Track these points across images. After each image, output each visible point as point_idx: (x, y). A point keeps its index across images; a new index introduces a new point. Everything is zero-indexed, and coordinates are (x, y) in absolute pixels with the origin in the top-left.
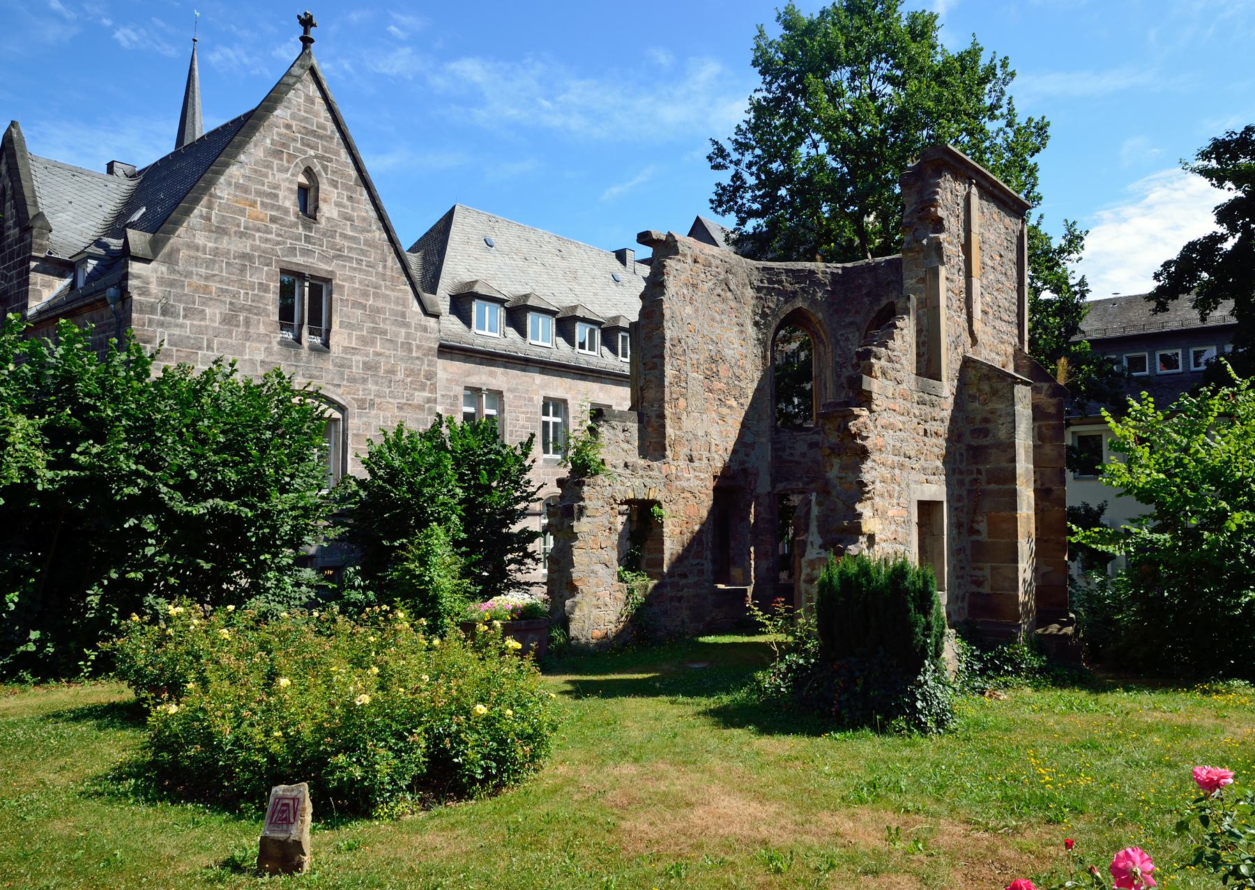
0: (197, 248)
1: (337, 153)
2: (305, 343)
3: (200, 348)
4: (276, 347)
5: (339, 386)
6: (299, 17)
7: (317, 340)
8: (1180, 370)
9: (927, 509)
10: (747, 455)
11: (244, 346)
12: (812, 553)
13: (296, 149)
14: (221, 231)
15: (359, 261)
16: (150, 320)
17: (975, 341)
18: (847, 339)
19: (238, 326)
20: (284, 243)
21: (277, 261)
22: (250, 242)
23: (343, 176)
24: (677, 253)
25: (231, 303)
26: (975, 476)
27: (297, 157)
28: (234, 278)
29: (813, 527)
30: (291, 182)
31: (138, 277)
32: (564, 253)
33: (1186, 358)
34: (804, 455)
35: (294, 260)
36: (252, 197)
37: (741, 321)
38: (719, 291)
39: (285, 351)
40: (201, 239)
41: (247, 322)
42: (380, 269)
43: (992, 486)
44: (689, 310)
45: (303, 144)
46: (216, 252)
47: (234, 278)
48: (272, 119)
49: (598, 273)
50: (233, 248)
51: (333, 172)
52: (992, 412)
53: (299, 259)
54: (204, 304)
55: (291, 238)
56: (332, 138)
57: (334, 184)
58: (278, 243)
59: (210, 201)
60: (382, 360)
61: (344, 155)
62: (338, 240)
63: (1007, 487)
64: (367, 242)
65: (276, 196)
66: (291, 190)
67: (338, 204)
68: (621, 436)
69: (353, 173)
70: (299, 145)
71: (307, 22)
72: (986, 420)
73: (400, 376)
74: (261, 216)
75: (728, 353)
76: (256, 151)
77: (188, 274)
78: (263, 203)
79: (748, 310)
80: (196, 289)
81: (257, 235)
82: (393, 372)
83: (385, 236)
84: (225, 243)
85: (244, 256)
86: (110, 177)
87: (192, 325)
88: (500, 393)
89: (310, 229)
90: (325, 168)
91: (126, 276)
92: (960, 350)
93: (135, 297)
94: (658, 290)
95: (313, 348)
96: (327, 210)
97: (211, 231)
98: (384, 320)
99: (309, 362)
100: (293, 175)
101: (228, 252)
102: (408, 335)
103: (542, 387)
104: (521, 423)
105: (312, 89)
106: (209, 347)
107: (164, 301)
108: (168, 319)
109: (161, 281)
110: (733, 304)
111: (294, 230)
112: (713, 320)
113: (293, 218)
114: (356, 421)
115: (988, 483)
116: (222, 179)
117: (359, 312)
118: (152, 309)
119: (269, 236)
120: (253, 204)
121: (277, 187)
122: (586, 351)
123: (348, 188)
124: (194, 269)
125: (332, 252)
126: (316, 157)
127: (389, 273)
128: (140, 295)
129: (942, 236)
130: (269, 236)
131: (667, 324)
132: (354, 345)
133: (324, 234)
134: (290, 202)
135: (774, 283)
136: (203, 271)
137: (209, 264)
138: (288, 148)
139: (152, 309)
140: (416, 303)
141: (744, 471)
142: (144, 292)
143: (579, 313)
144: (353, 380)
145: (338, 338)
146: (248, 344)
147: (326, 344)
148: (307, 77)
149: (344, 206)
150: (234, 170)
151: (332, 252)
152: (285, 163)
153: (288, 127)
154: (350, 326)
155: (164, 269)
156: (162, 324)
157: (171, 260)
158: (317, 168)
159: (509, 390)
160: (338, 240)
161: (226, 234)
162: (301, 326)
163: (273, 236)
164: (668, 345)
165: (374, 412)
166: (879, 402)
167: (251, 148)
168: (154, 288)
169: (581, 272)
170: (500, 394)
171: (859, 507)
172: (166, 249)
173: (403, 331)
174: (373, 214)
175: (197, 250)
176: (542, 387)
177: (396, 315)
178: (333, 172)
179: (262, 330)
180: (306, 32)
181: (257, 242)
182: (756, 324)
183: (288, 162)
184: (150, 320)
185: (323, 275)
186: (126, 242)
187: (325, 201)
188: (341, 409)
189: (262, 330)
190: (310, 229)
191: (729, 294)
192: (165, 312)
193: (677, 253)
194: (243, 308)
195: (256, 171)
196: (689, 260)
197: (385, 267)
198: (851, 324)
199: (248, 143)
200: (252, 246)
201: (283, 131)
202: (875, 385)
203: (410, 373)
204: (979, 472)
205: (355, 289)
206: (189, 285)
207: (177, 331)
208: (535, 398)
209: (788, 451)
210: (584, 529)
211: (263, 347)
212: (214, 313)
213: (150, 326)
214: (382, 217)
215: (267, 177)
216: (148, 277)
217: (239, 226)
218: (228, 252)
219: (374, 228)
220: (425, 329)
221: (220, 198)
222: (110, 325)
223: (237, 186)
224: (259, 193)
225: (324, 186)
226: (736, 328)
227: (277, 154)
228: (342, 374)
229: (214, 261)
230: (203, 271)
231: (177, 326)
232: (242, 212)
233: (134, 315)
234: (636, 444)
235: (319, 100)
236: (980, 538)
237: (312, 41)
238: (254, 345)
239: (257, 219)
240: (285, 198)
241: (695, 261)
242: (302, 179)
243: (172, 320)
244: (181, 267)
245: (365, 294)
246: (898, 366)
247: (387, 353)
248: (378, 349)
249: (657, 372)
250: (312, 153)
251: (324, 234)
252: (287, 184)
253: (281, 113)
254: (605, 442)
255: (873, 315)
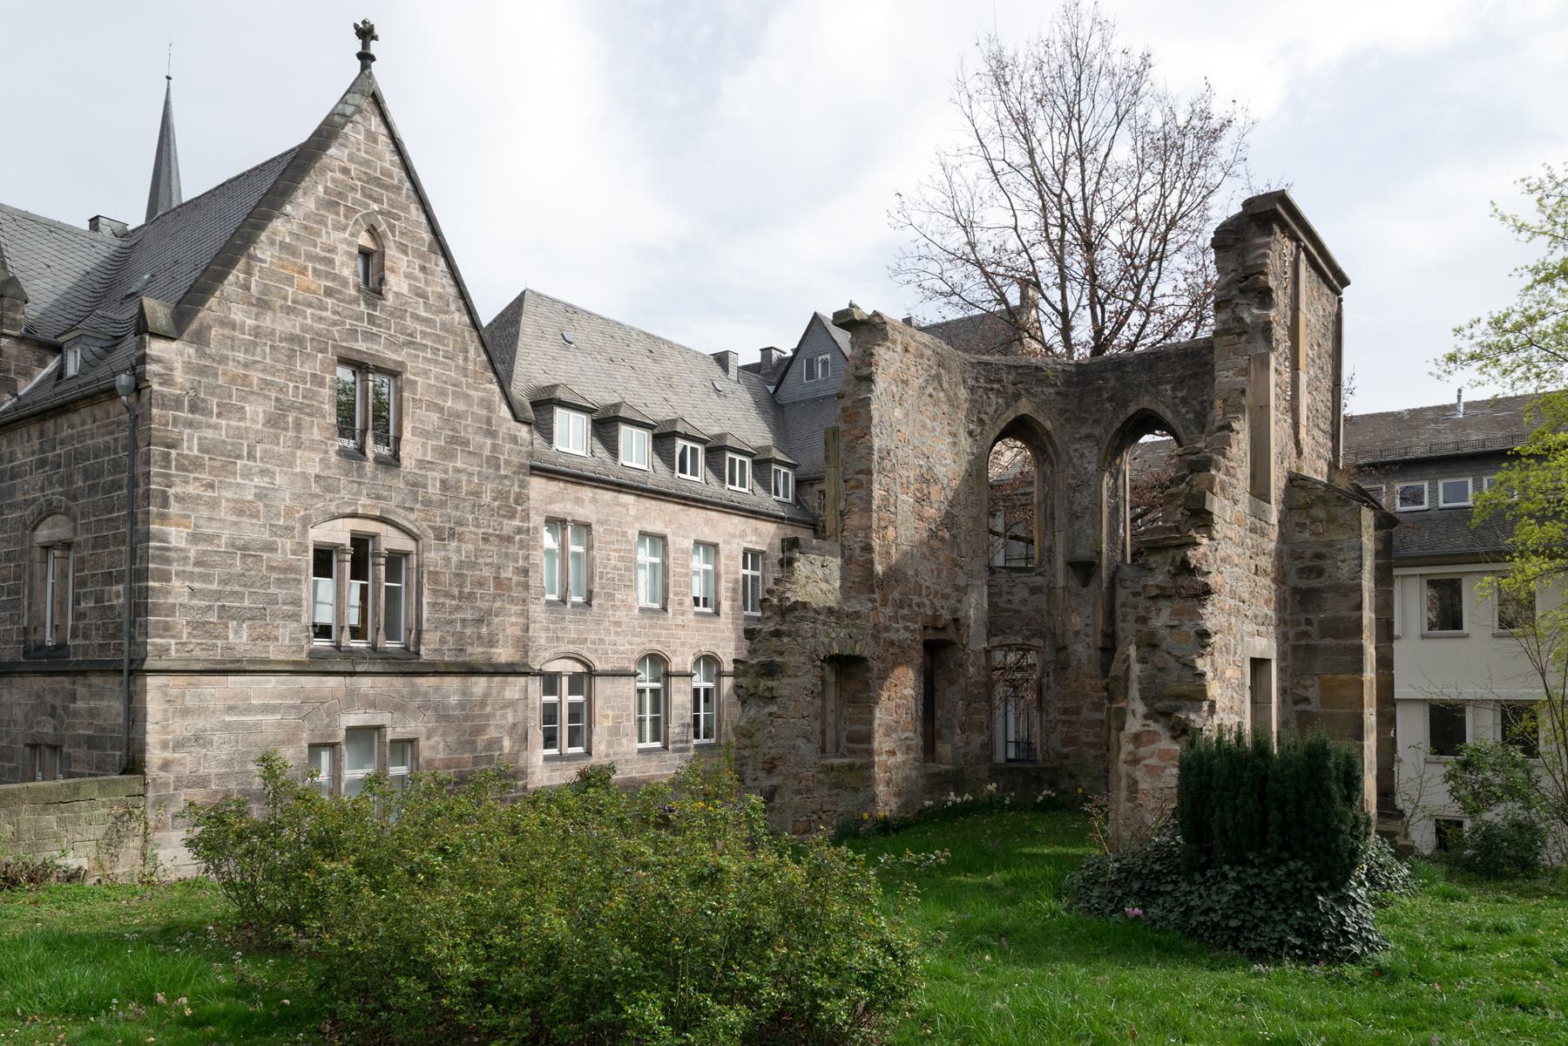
0: (233, 326)
1: (406, 209)
2: (370, 455)
3: (239, 457)
4: (334, 458)
5: (412, 509)
6: (356, 26)
7: (385, 451)
8: (1426, 506)
9: (1258, 665)
10: (959, 601)
11: (293, 455)
12: (1134, 725)
13: (355, 201)
14: (262, 305)
15: (435, 351)
16: (175, 419)
17: (1300, 453)
18: (1082, 456)
19: (286, 429)
20: (343, 323)
21: (334, 347)
22: (300, 319)
23: (415, 239)
24: (885, 338)
25: (277, 399)
26: (1303, 628)
27: (356, 211)
28: (280, 366)
29: (1134, 691)
30: (350, 244)
31: (158, 361)
32: (656, 355)
33: (1433, 491)
34: (1024, 602)
35: (356, 346)
36: (301, 261)
37: (953, 430)
38: (930, 390)
39: (344, 463)
40: (238, 314)
41: (298, 426)
42: (461, 362)
43: (1328, 641)
44: (898, 413)
45: (364, 195)
46: (257, 332)
47: (280, 366)
48: (325, 159)
49: (696, 381)
50: (279, 328)
51: (402, 233)
52: (1330, 544)
53: (361, 345)
54: (243, 399)
55: (351, 317)
56: (399, 189)
57: (403, 249)
58: (335, 324)
59: (248, 264)
60: (464, 478)
61: (415, 213)
62: (409, 321)
63: (1349, 642)
64: (444, 326)
65: (331, 262)
66: (350, 254)
67: (408, 276)
68: (819, 572)
69: (427, 236)
70: (359, 196)
71: (366, 33)
72: (1320, 556)
73: (486, 498)
74: (313, 287)
75: (940, 471)
76: (305, 202)
77: (223, 360)
78: (315, 270)
79: (961, 415)
80: (233, 380)
81: (309, 311)
82: (477, 494)
83: (466, 319)
84: (267, 321)
85: (293, 339)
86: (93, 235)
87: (228, 426)
88: (588, 526)
89: (374, 306)
90: (392, 228)
91: (143, 359)
92: (1286, 465)
93: (156, 387)
94: (863, 385)
95: (379, 460)
96: (396, 284)
97: (250, 304)
98: (466, 427)
99: (375, 477)
100: (352, 235)
101: (273, 332)
102: (494, 447)
103: (637, 519)
104: (613, 562)
105: (375, 123)
106: (251, 456)
107: (192, 393)
108: (198, 417)
109: (189, 367)
110: (945, 408)
111: (355, 307)
112: (924, 427)
113: (352, 292)
114: (432, 555)
115: (1323, 637)
116: (263, 237)
117: (435, 416)
118: (177, 403)
119: (324, 314)
120: (303, 271)
121: (332, 250)
122: (688, 476)
123: (421, 256)
124: (230, 353)
125: (402, 338)
126: (380, 212)
127: (471, 367)
128: (161, 384)
129: (1272, 313)
130: (324, 314)
131: (875, 430)
132: (429, 458)
133: (391, 314)
134: (349, 270)
135: (991, 381)
136: (241, 356)
137: (250, 347)
138: (346, 199)
139: (177, 403)
140: (504, 407)
141: (956, 620)
142: (167, 380)
143: (680, 428)
144: (428, 503)
145: (412, 450)
146: (299, 453)
147: (396, 456)
148: (366, 104)
149: (415, 279)
150: (277, 224)
151: (402, 338)
152: (342, 218)
153: (345, 171)
154: (426, 434)
155: (191, 351)
156: (190, 424)
157: (200, 339)
158: (383, 227)
159: (599, 522)
160: (409, 321)
161: (270, 308)
162: (364, 432)
163: (328, 314)
164: (876, 457)
165: (454, 544)
166: (1220, 529)
167: (299, 197)
168: (179, 376)
169: (675, 380)
170: (587, 526)
171: (1201, 664)
172: (194, 326)
173: (489, 442)
174: (452, 291)
175: (234, 328)
176: (637, 519)
177: (480, 421)
178: (402, 233)
179: (316, 435)
180: (365, 45)
181: (309, 321)
182: (971, 433)
183: (346, 217)
184: (175, 419)
185: (391, 366)
186: (141, 309)
187: (392, 271)
188: (415, 538)
189: (316, 435)
190: (374, 306)
191: (942, 394)
192: (194, 408)
193: (885, 338)
194: (292, 407)
195: (306, 228)
196: (899, 348)
197: (466, 359)
198: (1088, 437)
199: (295, 189)
200: (302, 325)
201: (339, 176)
202: (1217, 505)
203: (500, 495)
204: (1308, 622)
205: (430, 386)
206: (225, 374)
207: (209, 434)
208: (630, 532)
209: (1005, 597)
210: (785, 692)
211: (317, 457)
212: (256, 411)
213: (174, 425)
214: (463, 294)
215: (319, 234)
216: (170, 361)
217: (285, 298)
218: (273, 332)
219: (453, 308)
220: (514, 440)
221: (262, 261)
222: (119, 423)
223: (284, 246)
224: (311, 257)
225: (391, 252)
226: (949, 440)
227: (332, 205)
228: (416, 494)
229: (255, 344)
230: (241, 356)
231: (209, 426)
232: (289, 280)
233: (155, 411)
234: (838, 584)
235: (383, 139)
236: (1309, 708)
237: (373, 59)
238: (307, 454)
239: (308, 290)
240: (342, 264)
241: (906, 350)
242: (364, 240)
243: (203, 419)
244: (212, 349)
245: (443, 393)
246: (1234, 481)
247: (470, 469)
248: (459, 464)
249: (863, 493)
250: (375, 207)
251: (391, 314)
252: (345, 247)
253: (335, 153)
254: (803, 581)
255: (1118, 425)
